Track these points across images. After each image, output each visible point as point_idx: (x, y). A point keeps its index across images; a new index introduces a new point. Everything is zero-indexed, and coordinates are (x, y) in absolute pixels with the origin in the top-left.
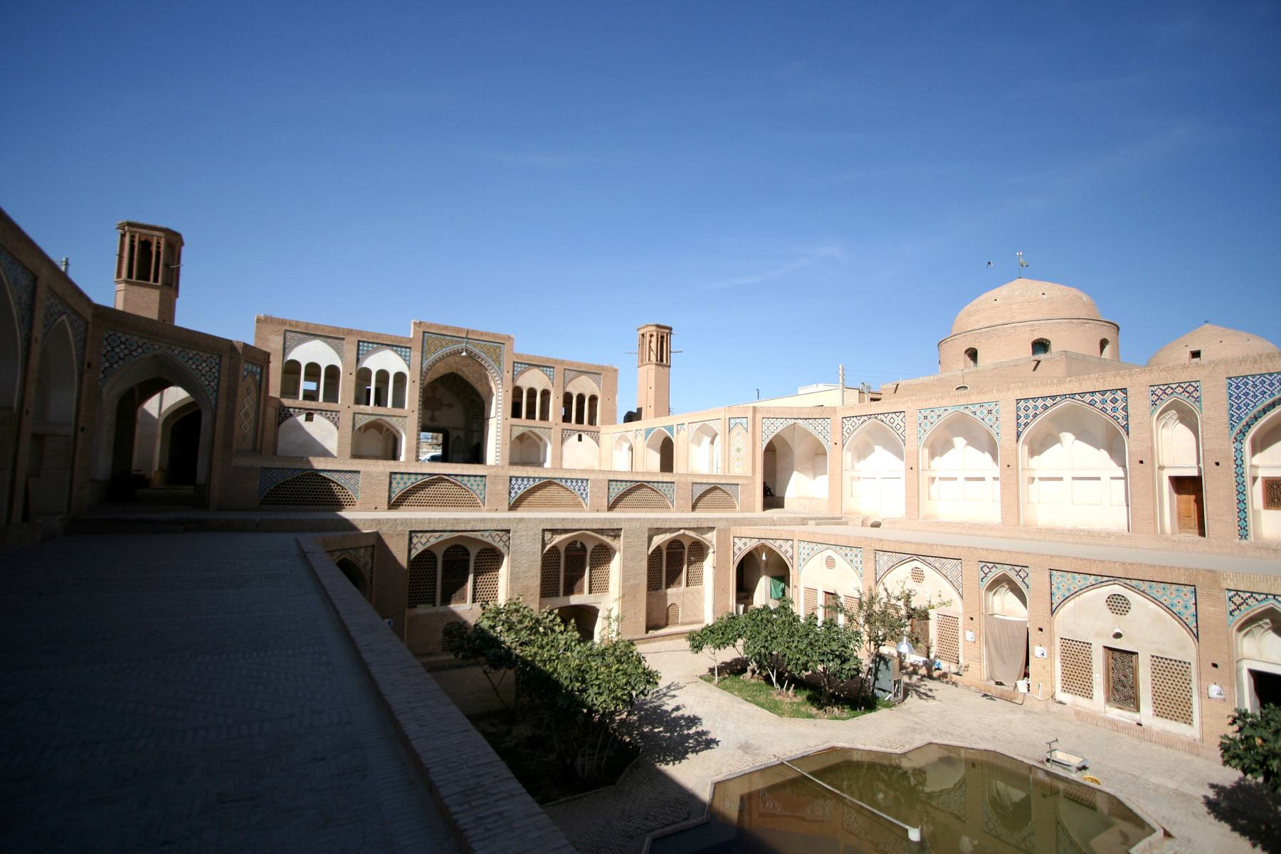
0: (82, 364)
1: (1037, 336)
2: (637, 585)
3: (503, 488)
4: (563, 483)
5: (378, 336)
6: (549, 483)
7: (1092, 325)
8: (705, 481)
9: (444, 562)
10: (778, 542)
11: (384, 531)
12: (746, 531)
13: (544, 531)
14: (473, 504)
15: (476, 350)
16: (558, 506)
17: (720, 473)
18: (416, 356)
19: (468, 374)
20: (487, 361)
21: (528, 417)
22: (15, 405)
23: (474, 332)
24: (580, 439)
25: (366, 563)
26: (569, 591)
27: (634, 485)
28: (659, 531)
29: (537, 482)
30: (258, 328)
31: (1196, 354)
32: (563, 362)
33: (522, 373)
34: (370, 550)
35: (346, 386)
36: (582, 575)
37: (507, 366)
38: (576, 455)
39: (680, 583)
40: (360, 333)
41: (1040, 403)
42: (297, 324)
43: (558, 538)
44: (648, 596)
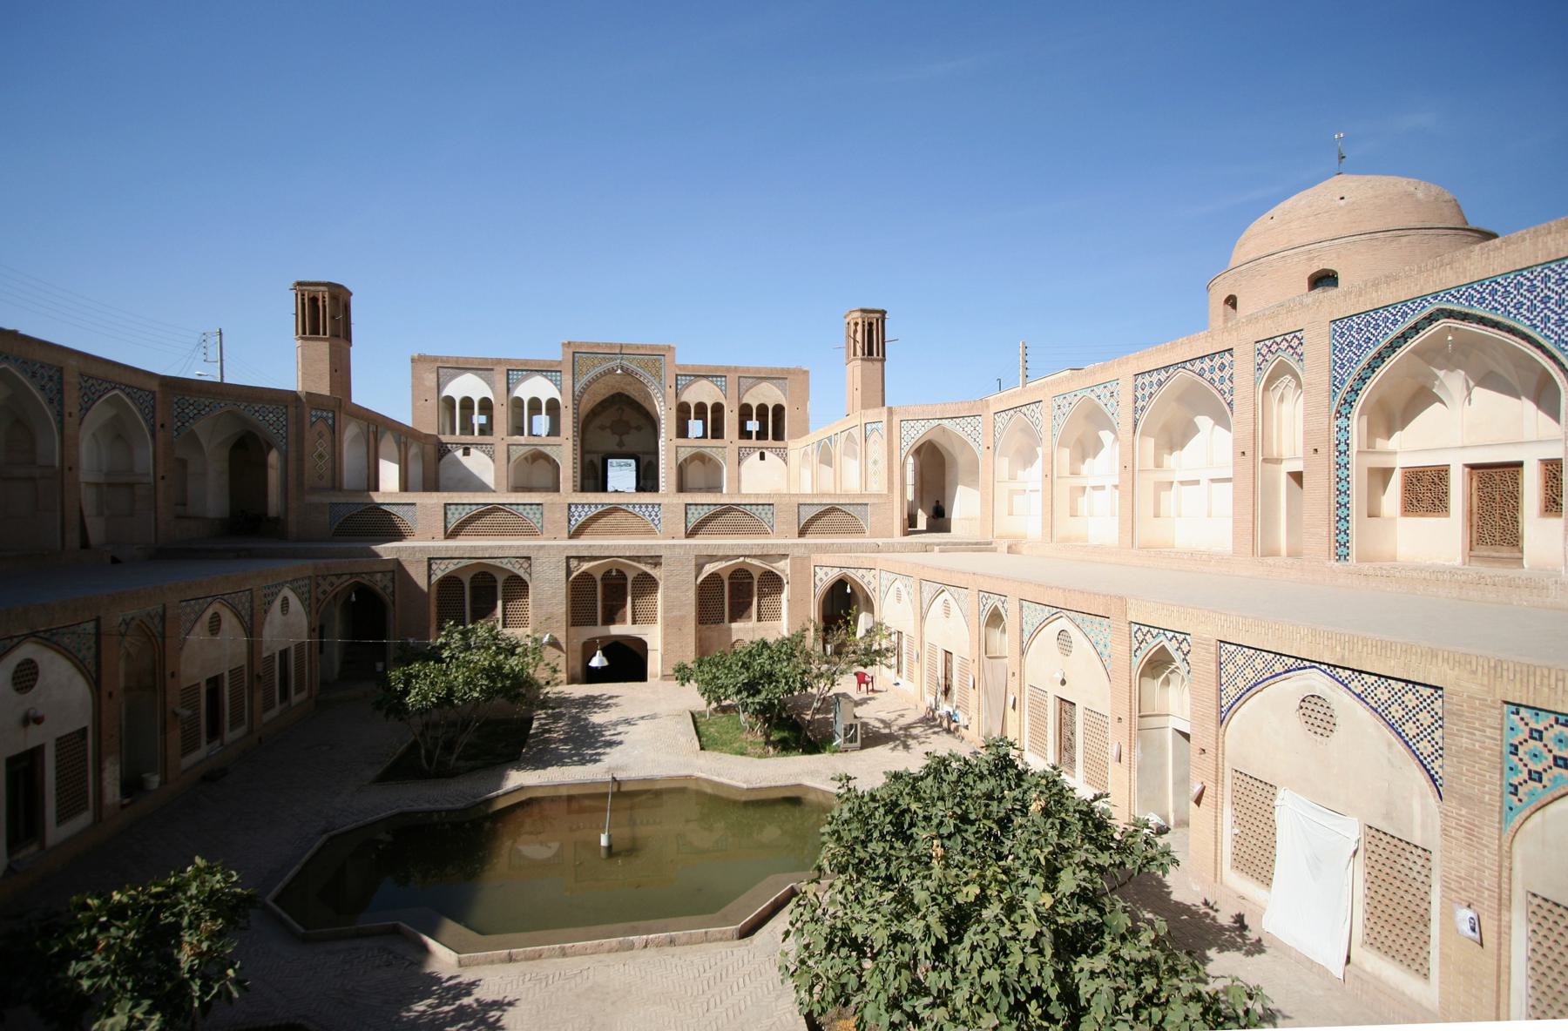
0: (153, 426)
1: (1316, 267)
2: (683, 617)
4: (630, 509)
5: (526, 362)
6: (728, 509)
7: (1414, 237)
8: (816, 501)
9: (473, 588)
11: (403, 558)
13: (568, 558)
14: (532, 532)
15: (633, 366)
16: (633, 533)
18: (567, 379)
20: (646, 377)
22: (57, 464)
23: (628, 346)
24: (762, 457)
26: (610, 619)
27: (719, 508)
28: (712, 558)
29: (600, 509)
30: (413, 368)
31: (1324, 279)
32: (736, 369)
33: (687, 386)
34: (390, 575)
36: (624, 605)
38: (757, 476)
39: (750, 617)
40: (507, 361)
42: (448, 359)
43: (585, 566)
44: (697, 631)
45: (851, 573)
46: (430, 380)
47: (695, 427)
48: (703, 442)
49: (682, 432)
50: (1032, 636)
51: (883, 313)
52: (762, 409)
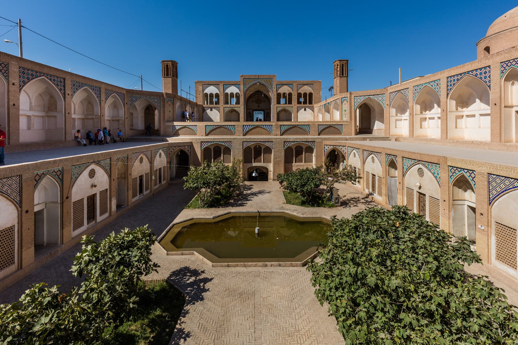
3: (241, 129)
5: (229, 82)
6: (295, 126)
8: (324, 124)
10: (341, 147)
11: (193, 141)
12: (328, 143)
15: (263, 82)
17: (321, 120)
18: (242, 87)
19: (262, 89)
21: (309, 104)
23: (261, 76)
24: (305, 110)
25: (188, 150)
29: (253, 127)
32: (296, 82)
35: (222, 98)
37: (274, 86)
41: (456, 78)
44: (285, 166)
45: (337, 147)
46: (200, 88)
47: (283, 101)
48: (285, 105)
49: (279, 102)
50: (408, 170)
51: (347, 61)
52: (305, 94)
